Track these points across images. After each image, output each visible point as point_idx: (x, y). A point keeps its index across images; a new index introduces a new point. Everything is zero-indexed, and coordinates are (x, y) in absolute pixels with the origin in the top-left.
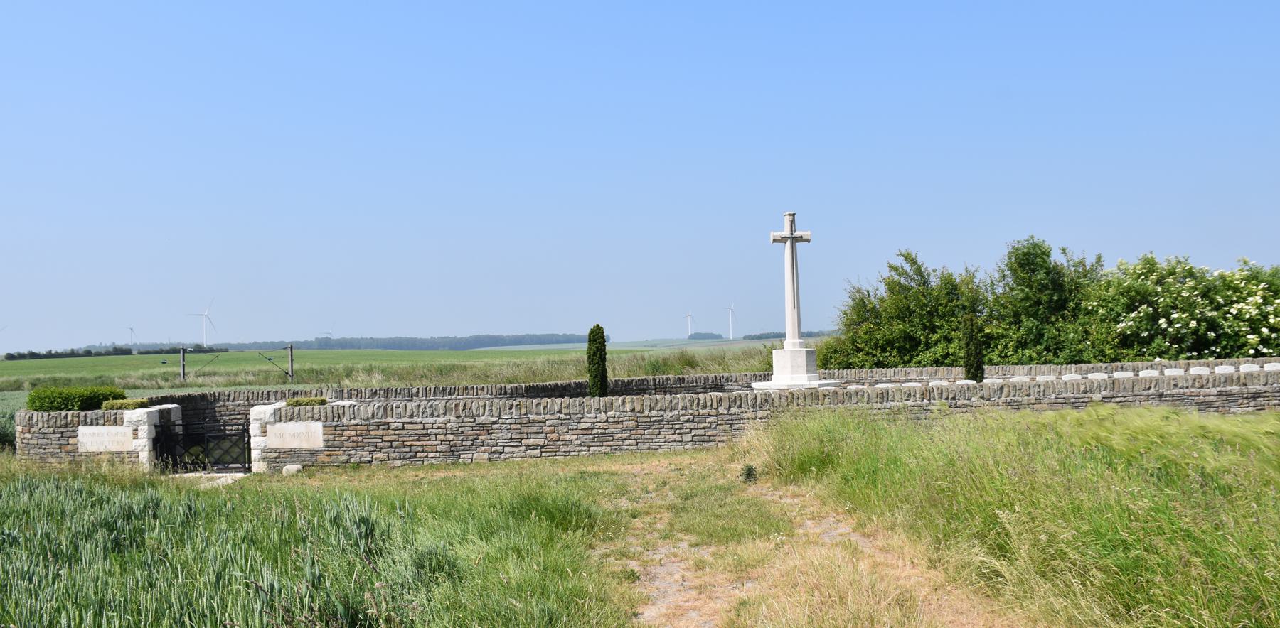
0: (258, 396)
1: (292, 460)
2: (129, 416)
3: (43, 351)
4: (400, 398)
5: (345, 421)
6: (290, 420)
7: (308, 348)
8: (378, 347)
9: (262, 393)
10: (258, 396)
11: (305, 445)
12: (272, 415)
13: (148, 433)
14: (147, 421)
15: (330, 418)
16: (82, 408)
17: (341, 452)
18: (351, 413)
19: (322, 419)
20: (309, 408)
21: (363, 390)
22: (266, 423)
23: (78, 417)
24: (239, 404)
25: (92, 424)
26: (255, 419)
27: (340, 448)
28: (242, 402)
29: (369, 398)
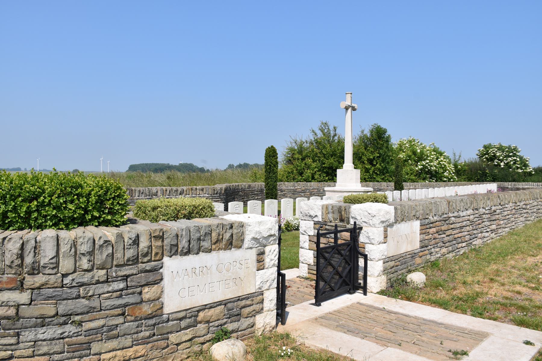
25: (188, 252)
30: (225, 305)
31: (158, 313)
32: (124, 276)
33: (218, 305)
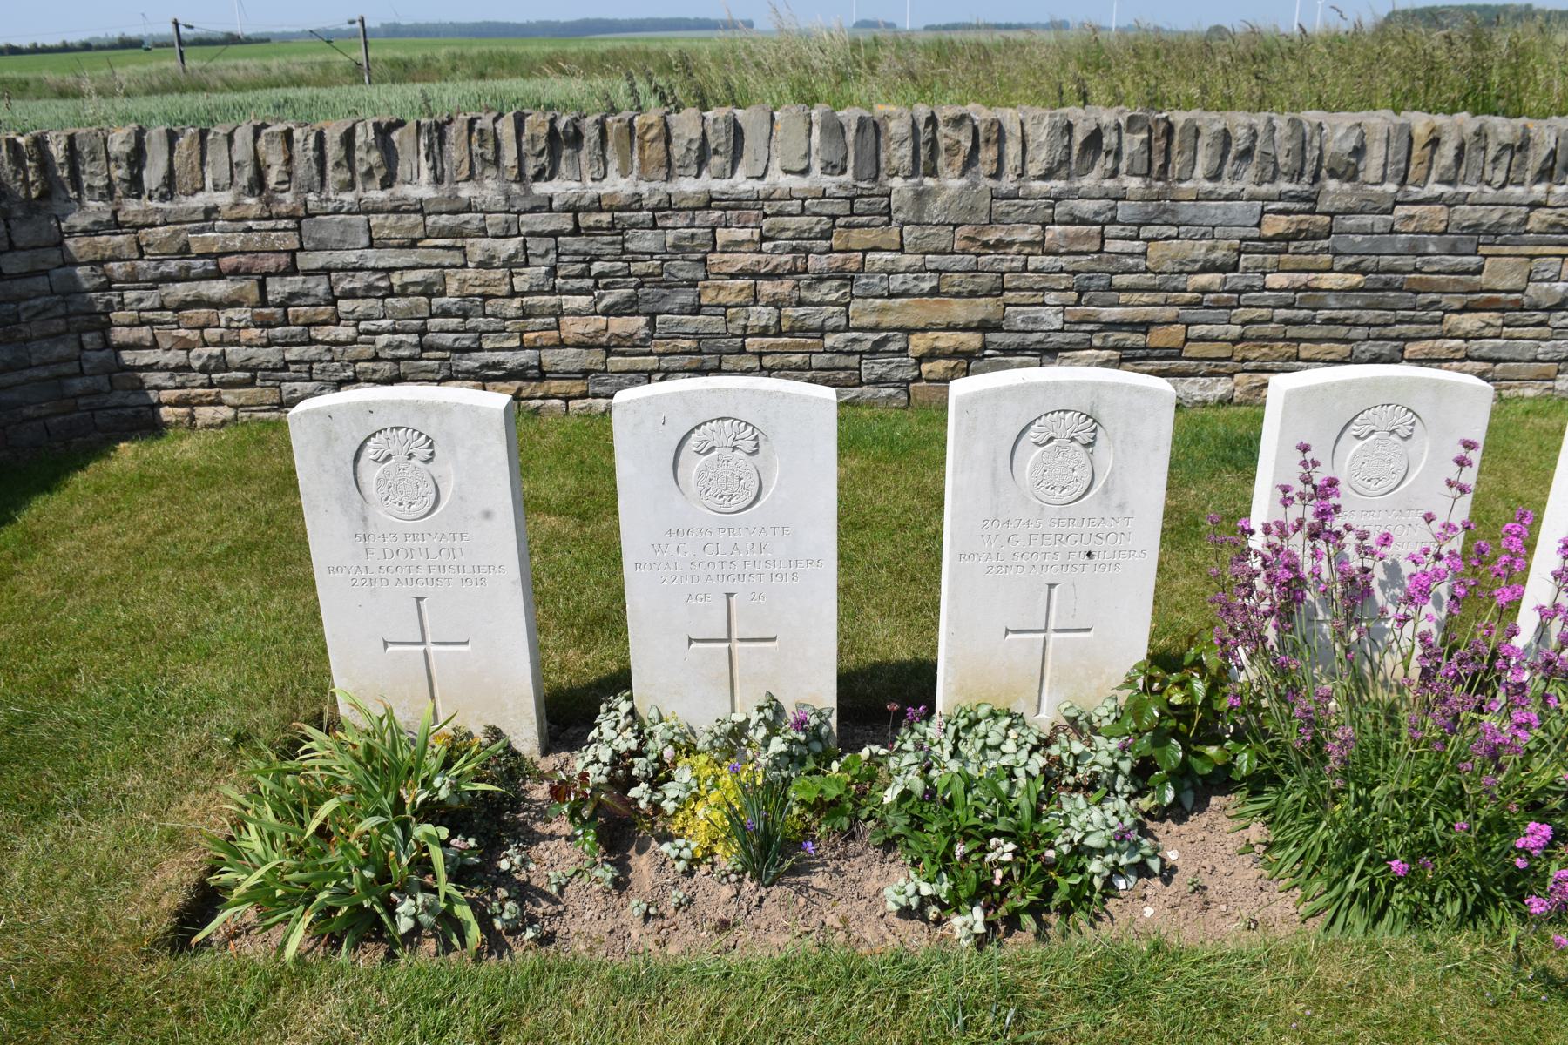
0: (321, 160)
4: (1246, 184)
9: (348, 139)
10: (321, 160)
24: (210, 213)
28: (224, 199)
29: (1047, 175)
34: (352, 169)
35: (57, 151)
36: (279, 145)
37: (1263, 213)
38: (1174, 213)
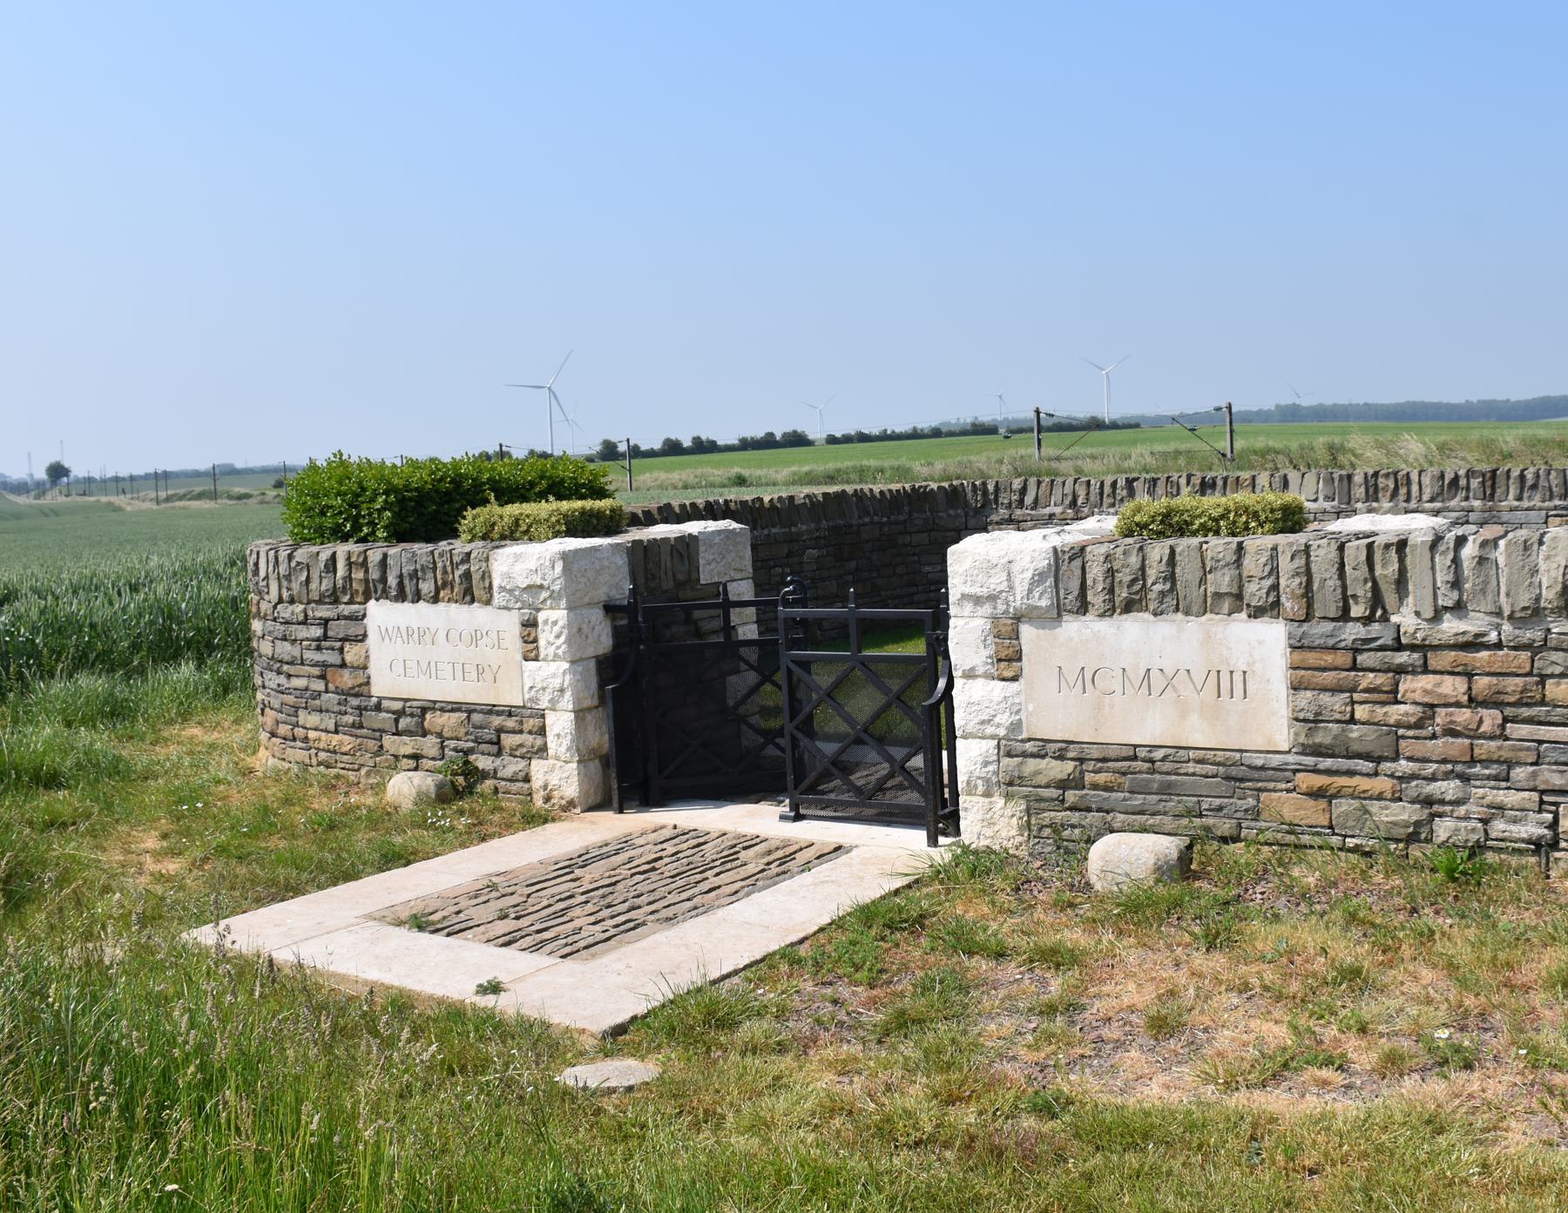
0: (1101, 494)
1: (1138, 800)
2: (505, 569)
3: (875, 431)
4: (1536, 502)
5: (1406, 619)
6: (1128, 607)
7: (1266, 421)
8: (1377, 418)
9: (1114, 484)
10: (1101, 494)
11: (1199, 734)
12: (1038, 578)
13: (569, 641)
14: (565, 588)
15: (1327, 602)
16: (400, 535)
17: (1383, 784)
18: (1442, 577)
19: (1287, 603)
20: (1218, 545)
21: (1414, 477)
22: (1018, 618)
23: (364, 564)
25: (401, 596)
26: (964, 597)
27: (1379, 760)
28: (1058, 510)
29: (1432, 500)
30: (470, 712)
31: (361, 690)
32: (320, 619)
33: (452, 710)
34: (1114, 498)
35: (991, 487)
36: (1084, 487)
37: (1547, 517)
38: (1499, 518)
